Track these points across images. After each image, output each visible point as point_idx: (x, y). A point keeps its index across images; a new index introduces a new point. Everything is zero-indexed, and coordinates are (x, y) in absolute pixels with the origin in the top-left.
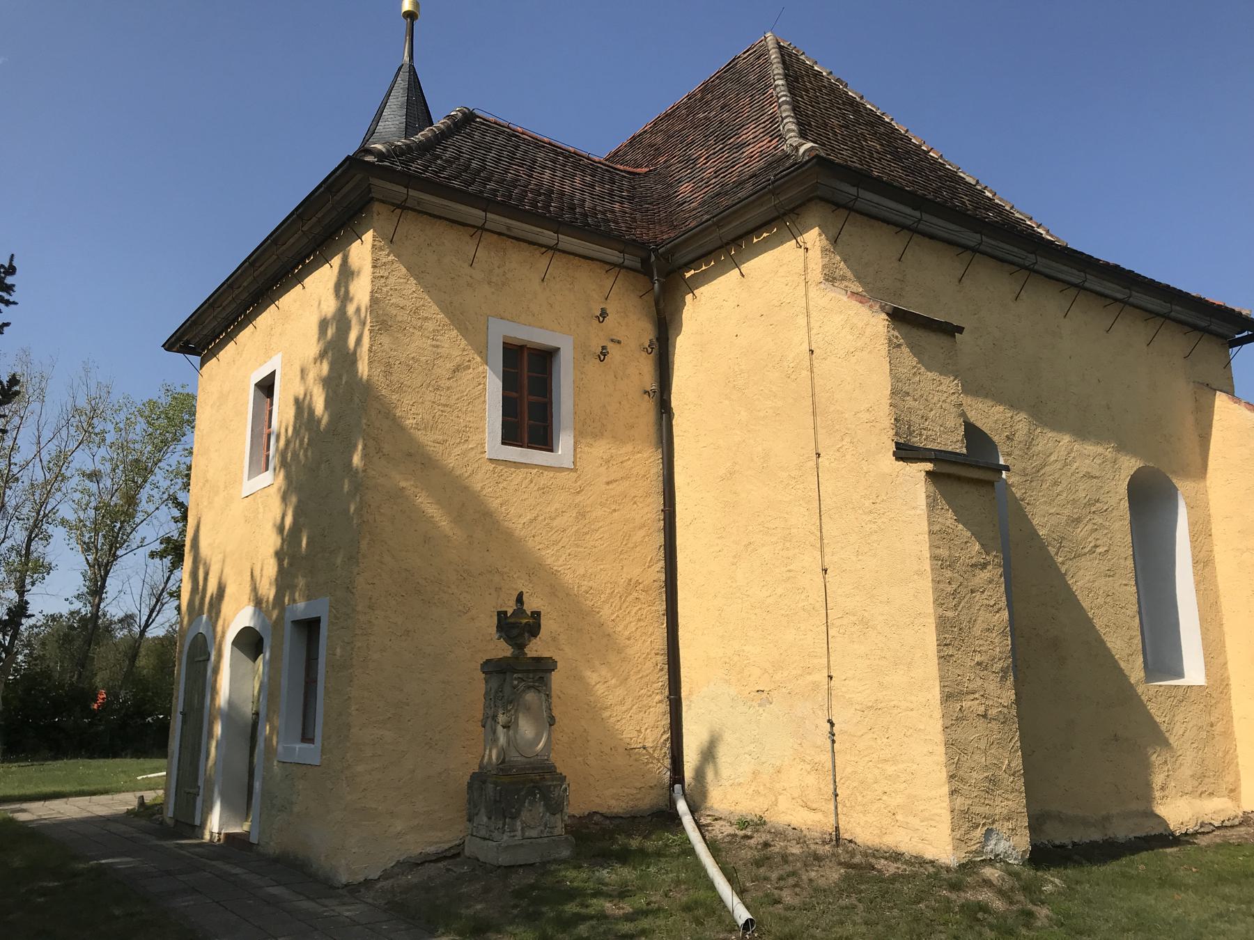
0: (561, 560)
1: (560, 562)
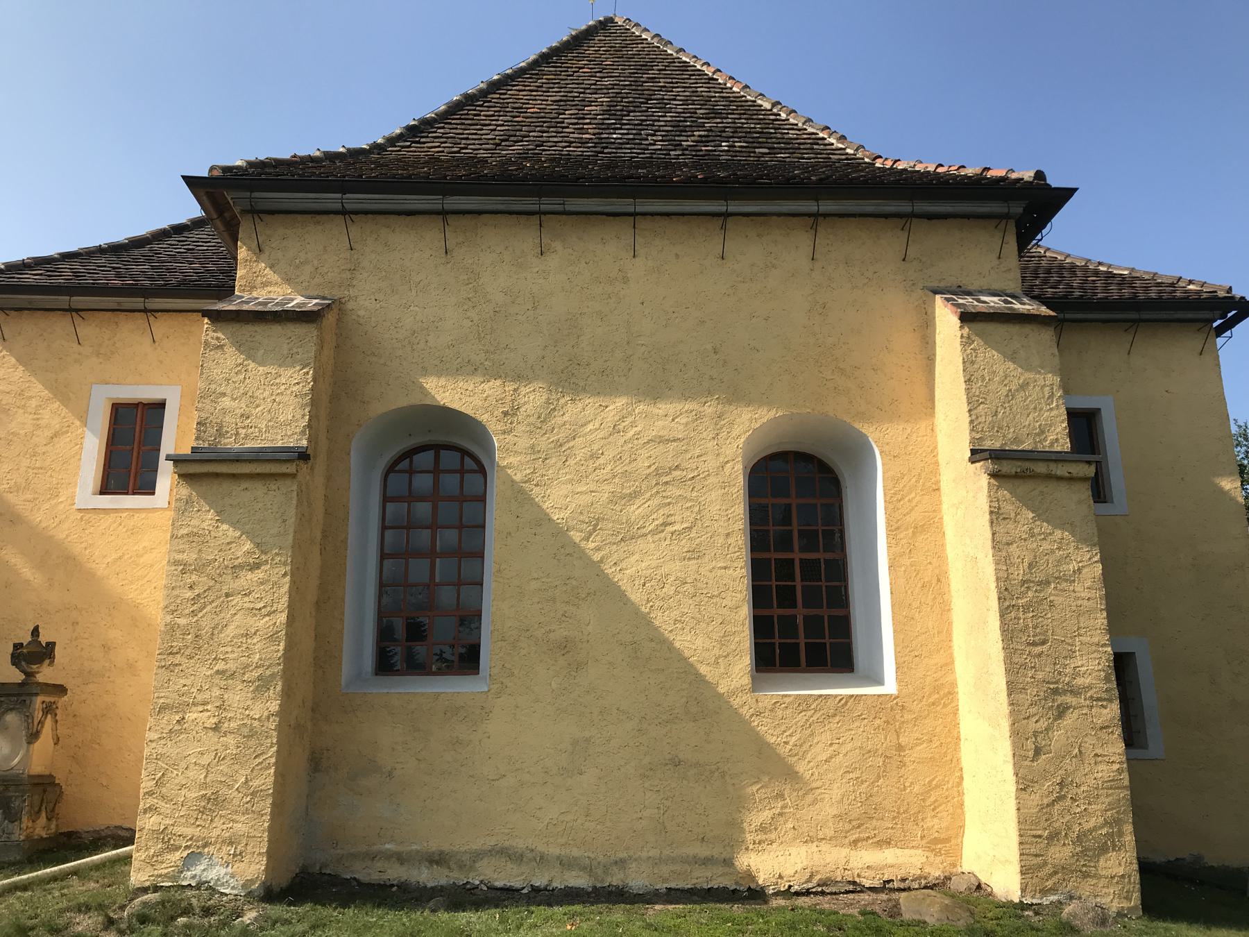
0: (145, 593)
1: (145, 595)
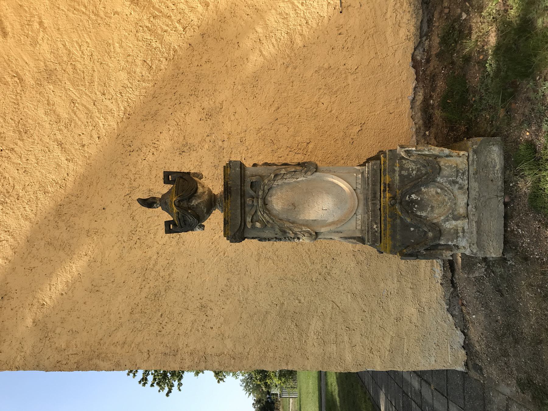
0: (111, 106)
